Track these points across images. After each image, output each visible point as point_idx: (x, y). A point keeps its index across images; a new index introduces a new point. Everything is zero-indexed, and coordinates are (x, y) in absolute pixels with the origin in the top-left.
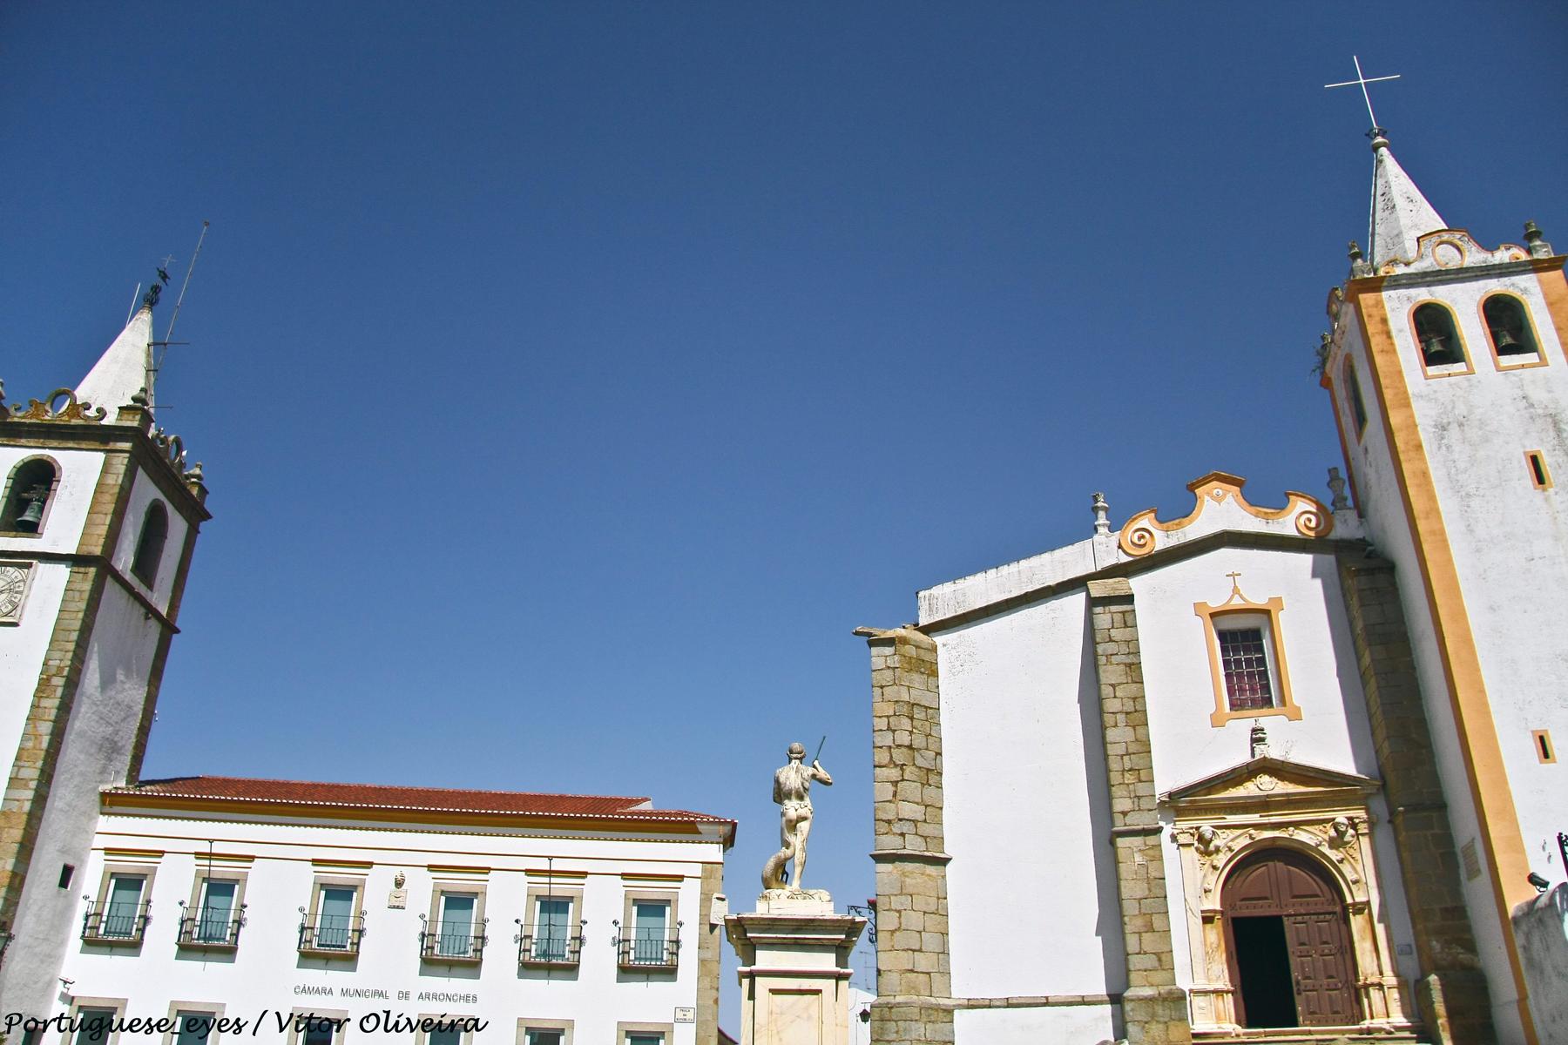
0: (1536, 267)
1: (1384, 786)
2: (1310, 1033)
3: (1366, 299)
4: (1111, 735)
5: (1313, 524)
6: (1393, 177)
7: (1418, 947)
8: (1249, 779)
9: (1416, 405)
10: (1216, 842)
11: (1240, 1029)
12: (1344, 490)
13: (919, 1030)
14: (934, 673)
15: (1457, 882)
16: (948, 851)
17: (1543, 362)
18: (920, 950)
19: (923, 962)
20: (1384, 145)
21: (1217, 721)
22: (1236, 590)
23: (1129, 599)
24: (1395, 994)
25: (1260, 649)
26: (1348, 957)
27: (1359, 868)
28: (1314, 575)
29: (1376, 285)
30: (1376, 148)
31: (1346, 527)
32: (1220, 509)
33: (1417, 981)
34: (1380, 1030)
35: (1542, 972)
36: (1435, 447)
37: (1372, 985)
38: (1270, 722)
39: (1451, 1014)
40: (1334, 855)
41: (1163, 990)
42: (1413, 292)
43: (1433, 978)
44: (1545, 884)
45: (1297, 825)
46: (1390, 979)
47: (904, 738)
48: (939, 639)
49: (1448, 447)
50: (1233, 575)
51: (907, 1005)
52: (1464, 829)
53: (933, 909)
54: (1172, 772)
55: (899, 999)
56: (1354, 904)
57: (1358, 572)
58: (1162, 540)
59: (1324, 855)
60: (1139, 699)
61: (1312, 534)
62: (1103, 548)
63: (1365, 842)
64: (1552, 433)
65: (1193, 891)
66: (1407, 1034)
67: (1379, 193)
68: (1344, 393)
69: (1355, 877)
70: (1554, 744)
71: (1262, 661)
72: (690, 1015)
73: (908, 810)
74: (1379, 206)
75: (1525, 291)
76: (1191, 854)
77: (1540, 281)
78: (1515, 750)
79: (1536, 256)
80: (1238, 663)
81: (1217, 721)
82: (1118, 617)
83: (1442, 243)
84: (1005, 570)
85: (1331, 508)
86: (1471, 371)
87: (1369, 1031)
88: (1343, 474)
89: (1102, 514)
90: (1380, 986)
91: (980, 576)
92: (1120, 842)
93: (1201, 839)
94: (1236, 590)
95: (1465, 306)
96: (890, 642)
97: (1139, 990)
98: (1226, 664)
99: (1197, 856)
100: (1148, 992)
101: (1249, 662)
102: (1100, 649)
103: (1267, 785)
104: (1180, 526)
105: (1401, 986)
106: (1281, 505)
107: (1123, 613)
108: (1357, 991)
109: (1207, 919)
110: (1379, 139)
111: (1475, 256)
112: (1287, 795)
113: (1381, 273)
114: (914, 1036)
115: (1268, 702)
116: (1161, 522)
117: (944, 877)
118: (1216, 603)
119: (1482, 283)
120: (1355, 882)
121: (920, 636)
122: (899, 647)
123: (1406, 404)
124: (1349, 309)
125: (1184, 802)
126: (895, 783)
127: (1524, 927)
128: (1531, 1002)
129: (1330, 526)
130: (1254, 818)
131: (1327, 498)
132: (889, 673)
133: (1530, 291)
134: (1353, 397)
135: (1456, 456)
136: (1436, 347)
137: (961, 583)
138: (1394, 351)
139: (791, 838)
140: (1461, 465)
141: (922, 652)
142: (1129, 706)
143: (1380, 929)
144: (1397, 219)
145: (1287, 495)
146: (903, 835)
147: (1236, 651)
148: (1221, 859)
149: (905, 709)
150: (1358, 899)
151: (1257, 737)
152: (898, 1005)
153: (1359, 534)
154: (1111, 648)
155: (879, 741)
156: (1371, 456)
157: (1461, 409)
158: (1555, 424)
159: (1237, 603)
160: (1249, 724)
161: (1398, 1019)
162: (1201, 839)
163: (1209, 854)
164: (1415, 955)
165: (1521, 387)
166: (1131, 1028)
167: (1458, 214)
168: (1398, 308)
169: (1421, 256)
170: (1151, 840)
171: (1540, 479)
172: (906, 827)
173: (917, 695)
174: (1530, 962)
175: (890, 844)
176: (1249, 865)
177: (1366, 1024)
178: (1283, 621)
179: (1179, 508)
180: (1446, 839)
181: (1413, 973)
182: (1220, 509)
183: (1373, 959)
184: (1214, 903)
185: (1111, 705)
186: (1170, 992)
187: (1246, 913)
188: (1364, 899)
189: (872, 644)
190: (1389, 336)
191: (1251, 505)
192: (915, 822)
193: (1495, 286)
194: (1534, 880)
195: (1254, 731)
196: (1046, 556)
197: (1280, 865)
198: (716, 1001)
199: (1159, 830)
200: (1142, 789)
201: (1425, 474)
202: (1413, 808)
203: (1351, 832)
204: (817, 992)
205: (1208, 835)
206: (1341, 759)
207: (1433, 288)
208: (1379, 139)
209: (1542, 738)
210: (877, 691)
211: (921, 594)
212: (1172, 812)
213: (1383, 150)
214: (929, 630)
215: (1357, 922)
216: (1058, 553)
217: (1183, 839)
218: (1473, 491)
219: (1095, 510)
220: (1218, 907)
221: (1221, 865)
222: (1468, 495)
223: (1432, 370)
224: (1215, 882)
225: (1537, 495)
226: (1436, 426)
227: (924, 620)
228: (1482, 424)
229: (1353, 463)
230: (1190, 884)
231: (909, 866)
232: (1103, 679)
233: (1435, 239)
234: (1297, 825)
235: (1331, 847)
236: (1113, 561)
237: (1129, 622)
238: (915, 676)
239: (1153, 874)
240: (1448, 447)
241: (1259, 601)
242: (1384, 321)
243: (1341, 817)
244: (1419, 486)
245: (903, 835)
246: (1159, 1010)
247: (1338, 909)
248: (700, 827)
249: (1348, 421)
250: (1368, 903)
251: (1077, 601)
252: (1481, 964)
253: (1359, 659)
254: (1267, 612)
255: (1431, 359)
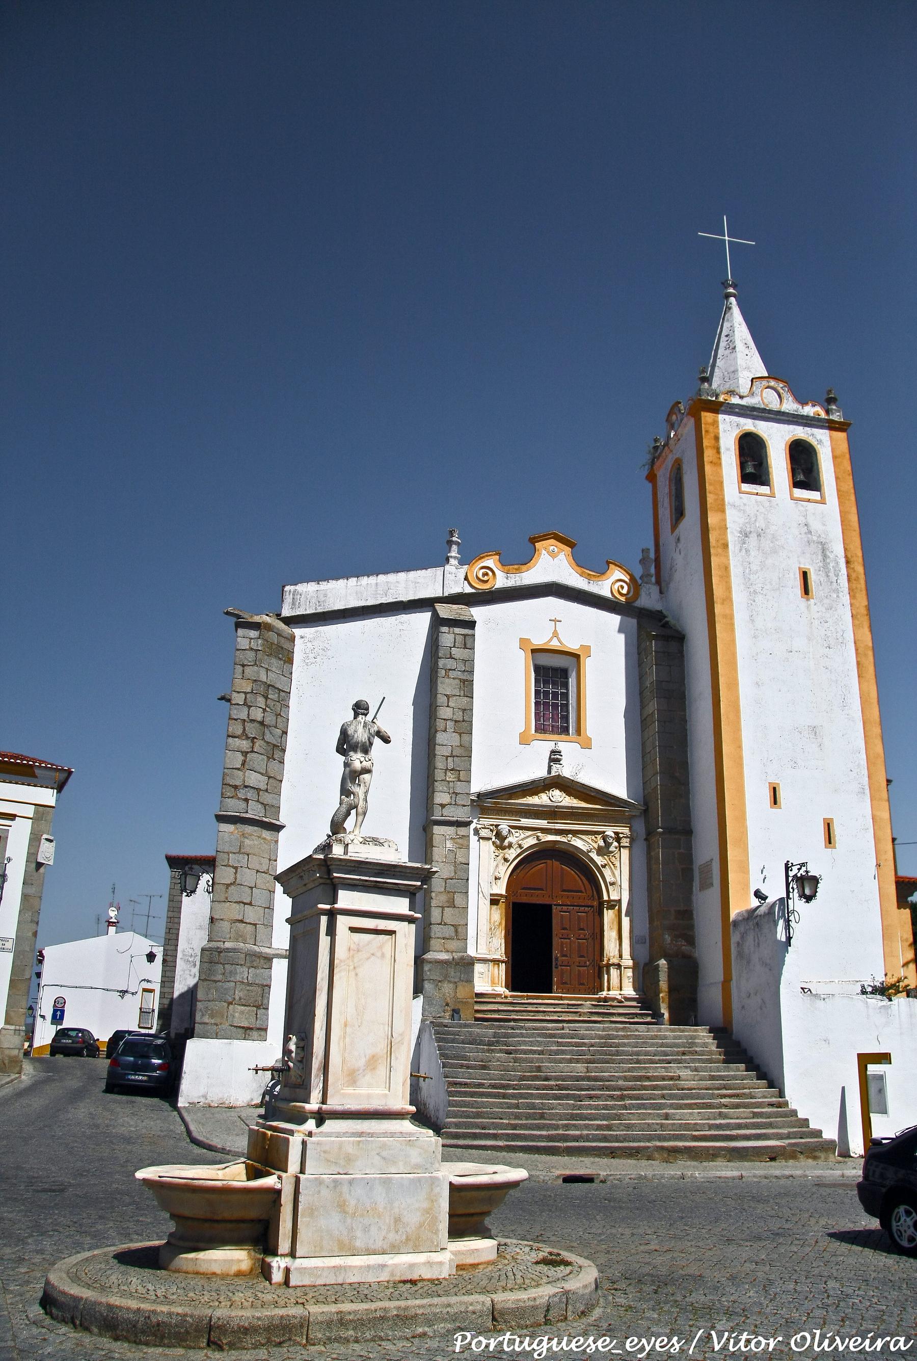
0: (832, 426)
1: (646, 812)
2: (561, 998)
3: (707, 417)
4: (441, 738)
5: (625, 591)
6: (736, 325)
7: (651, 938)
8: (543, 791)
9: (729, 512)
10: (510, 839)
11: (508, 993)
12: (655, 569)
13: (243, 973)
14: (290, 661)
15: (690, 891)
16: (283, 819)
17: (823, 501)
18: (250, 904)
19: (251, 914)
20: (734, 296)
21: (524, 740)
22: (555, 634)
23: (471, 624)
24: (630, 973)
25: (566, 685)
26: (597, 942)
27: (617, 873)
28: (620, 631)
29: (716, 407)
30: (728, 296)
31: (649, 600)
32: (552, 564)
33: (646, 965)
34: (614, 999)
35: (749, 962)
36: (737, 548)
37: (613, 965)
38: (568, 748)
39: (671, 990)
40: (599, 860)
41: (457, 956)
42: (742, 420)
43: (663, 962)
44: (764, 898)
45: (575, 833)
46: (627, 961)
47: (258, 714)
48: (298, 632)
49: (747, 551)
50: (555, 621)
51: (234, 950)
52: (705, 849)
53: (265, 868)
54: (484, 777)
55: (228, 945)
56: (609, 901)
57: (655, 637)
58: (502, 581)
59: (592, 860)
60: (468, 711)
61: (623, 599)
62: (452, 577)
63: (625, 853)
64: (820, 557)
65: (486, 878)
66: (634, 1004)
67: (724, 333)
68: (667, 490)
69: (613, 880)
70: (782, 795)
71: (566, 696)
72: (9, 945)
73: (254, 779)
74: (723, 344)
75: (820, 442)
76: (488, 847)
77: (831, 437)
78: (754, 795)
79: (831, 417)
80: (546, 694)
81: (524, 740)
82: (460, 639)
83: (768, 387)
84: (365, 580)
85: (640, 582)
86: (772, 495)
87: (606, 1000)
88: (652, 555)
89: (454, 547)
90: (619, 966)
91: (342, 582)
92: (437, 829)
93: (498, 835)
94: (555, 634)
95: (777, 440)
96: (256, 626)
97: (436, 955)
98: (537, 693)
99: (493, 848)
100: (444, 956)
101: (555, 695)
102: (441, 663)
103: (558, 798)
104: (518, 571)
105: (635, 968)
106: (601, 572)
107: (465, 636)
108: (600, 969)
109: (494, 901)
110: (731, 290)
111: (790, 405)
112: (572, 808)
113: (721, 399)
114: (238, 978)
115: (565, 730)
116: (503, 565)
117: (277, 842)
118: (540, 640)
119: (792, 427)
120: (612, 884)
121: (281, 625)
122: (264, 632)
123: (722, 509)
124: (690, 422)
125: (488, 803)
126: (245, 754)
127: (742, 929)
128: (734, 984)
129: (637, 595)
130: (543, 823)
131: (638, 572)
132: (251, 655)
133: (824, 443)
134: (676, 497)
135: (751, 559)
136: (750, 470)
137: (324, 586)
138: (720, 464)
139: (355, 789)
140: (754, 567)
141: (283, 640)
142: (459, 716)
143: (626, 921)
144: (735, 359)
145: (608, 563)
146: (246, 800)
147: (546, 683)
148: (512, 854)
149: (262, 689)
150: (612, 898)
151: (555, 758)
152: (228, 950)
153: (658, 607)
154: (450, 664)
155: (235, 713)
156: (680, 546)
157: (761, 523)
158: (824, 550)
159: (555, 644)
160: (549, 746)
161: (629, 991)
162: (498, 835)
163: (503, 848)
164: (647, 944)
165: (805, 516)
166: (427, 986)
167: (778, 369)
168: (729, 430)
169: (752, 394)
170: (462, 831)
171: (806, 590)
172: (250, 794)
173: (272, 678)
174: (740, 955)
175: (234, 807)
176: (532, 861)
177: (604, 994)
178: (589, 667)
179: (525, 559)
180: (687, 859)
181: (644, 957)
182: (552, 564)
183: (618, 944)
184: (501, 889)
185: (445, 713)
186: (462, 958)
187: (524, 900)
188: (617, 898)
189: (238, 625)
190: (718, 452)
191: (578, 566)
192: (258, 790)
193: (801, 432)
194: (758, 894)
195: (553, 752)
196: (402, 575)
197: (558, 863)
198: (35, 934)
199: (467, 824)
200: (460, 787)
201: (727, 568)
202: (669, 831)
203: (616, 844)
204: (391, 933)
205: (505, 833)
206: (615, 782)
207: (757, 422)
208: (731, 290)
209: (774, 789)
210: (239, 669)
211: (287, 588)
212: (478, 810)
213: (733, 300)
214: (293, 621)
215: (609, 916)
216: (412, 574)
217: (484, 833)
218: (759, 590)
219: (450, 543)
220: (504, 893)
221: (511, 858)
222: (755, 592)
223: (746, 487)
224: (504, 872)
225: (802, 602)
226: (741, 532)
227: (286, 612)
228: (774, 538)
229: (661, 549)
230: (487, 871)
231: (249, 829)
232: (441, 689)
233: (765, 383)
234: (575, 833)
235: (598, 854)
236: (459, 590)
237: (468, 643)
238: (274, 661)
239: (460, 859)
240: (747, 551)
241: (572, 645)
242: (717, 438)
243: (610, 832)
244: (721, 577)
245: (246, 800)
246: (452, 972)
247: (595, 903)
248: (37, 771)
249: (665, 513)
250: (620, 901)
251: (423, 619)
252: (696, 955)
253: (643, 707)
254: (577, 657)
255: (746, 478)
